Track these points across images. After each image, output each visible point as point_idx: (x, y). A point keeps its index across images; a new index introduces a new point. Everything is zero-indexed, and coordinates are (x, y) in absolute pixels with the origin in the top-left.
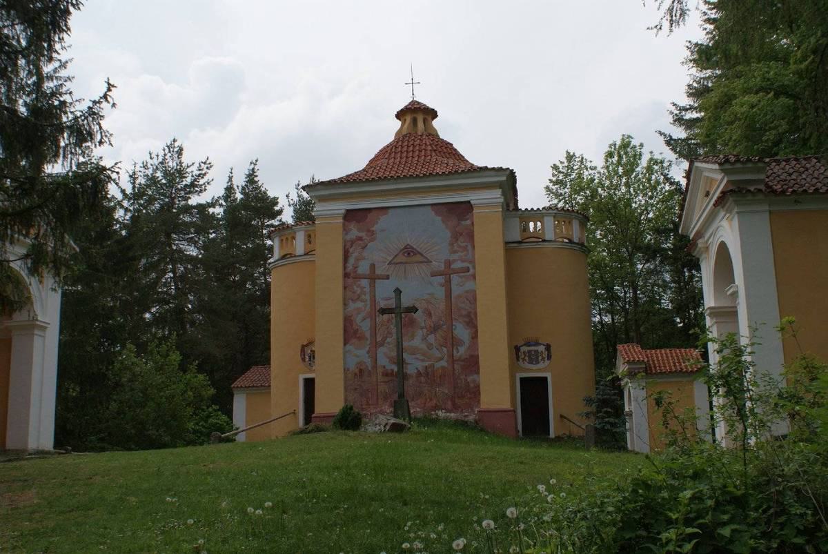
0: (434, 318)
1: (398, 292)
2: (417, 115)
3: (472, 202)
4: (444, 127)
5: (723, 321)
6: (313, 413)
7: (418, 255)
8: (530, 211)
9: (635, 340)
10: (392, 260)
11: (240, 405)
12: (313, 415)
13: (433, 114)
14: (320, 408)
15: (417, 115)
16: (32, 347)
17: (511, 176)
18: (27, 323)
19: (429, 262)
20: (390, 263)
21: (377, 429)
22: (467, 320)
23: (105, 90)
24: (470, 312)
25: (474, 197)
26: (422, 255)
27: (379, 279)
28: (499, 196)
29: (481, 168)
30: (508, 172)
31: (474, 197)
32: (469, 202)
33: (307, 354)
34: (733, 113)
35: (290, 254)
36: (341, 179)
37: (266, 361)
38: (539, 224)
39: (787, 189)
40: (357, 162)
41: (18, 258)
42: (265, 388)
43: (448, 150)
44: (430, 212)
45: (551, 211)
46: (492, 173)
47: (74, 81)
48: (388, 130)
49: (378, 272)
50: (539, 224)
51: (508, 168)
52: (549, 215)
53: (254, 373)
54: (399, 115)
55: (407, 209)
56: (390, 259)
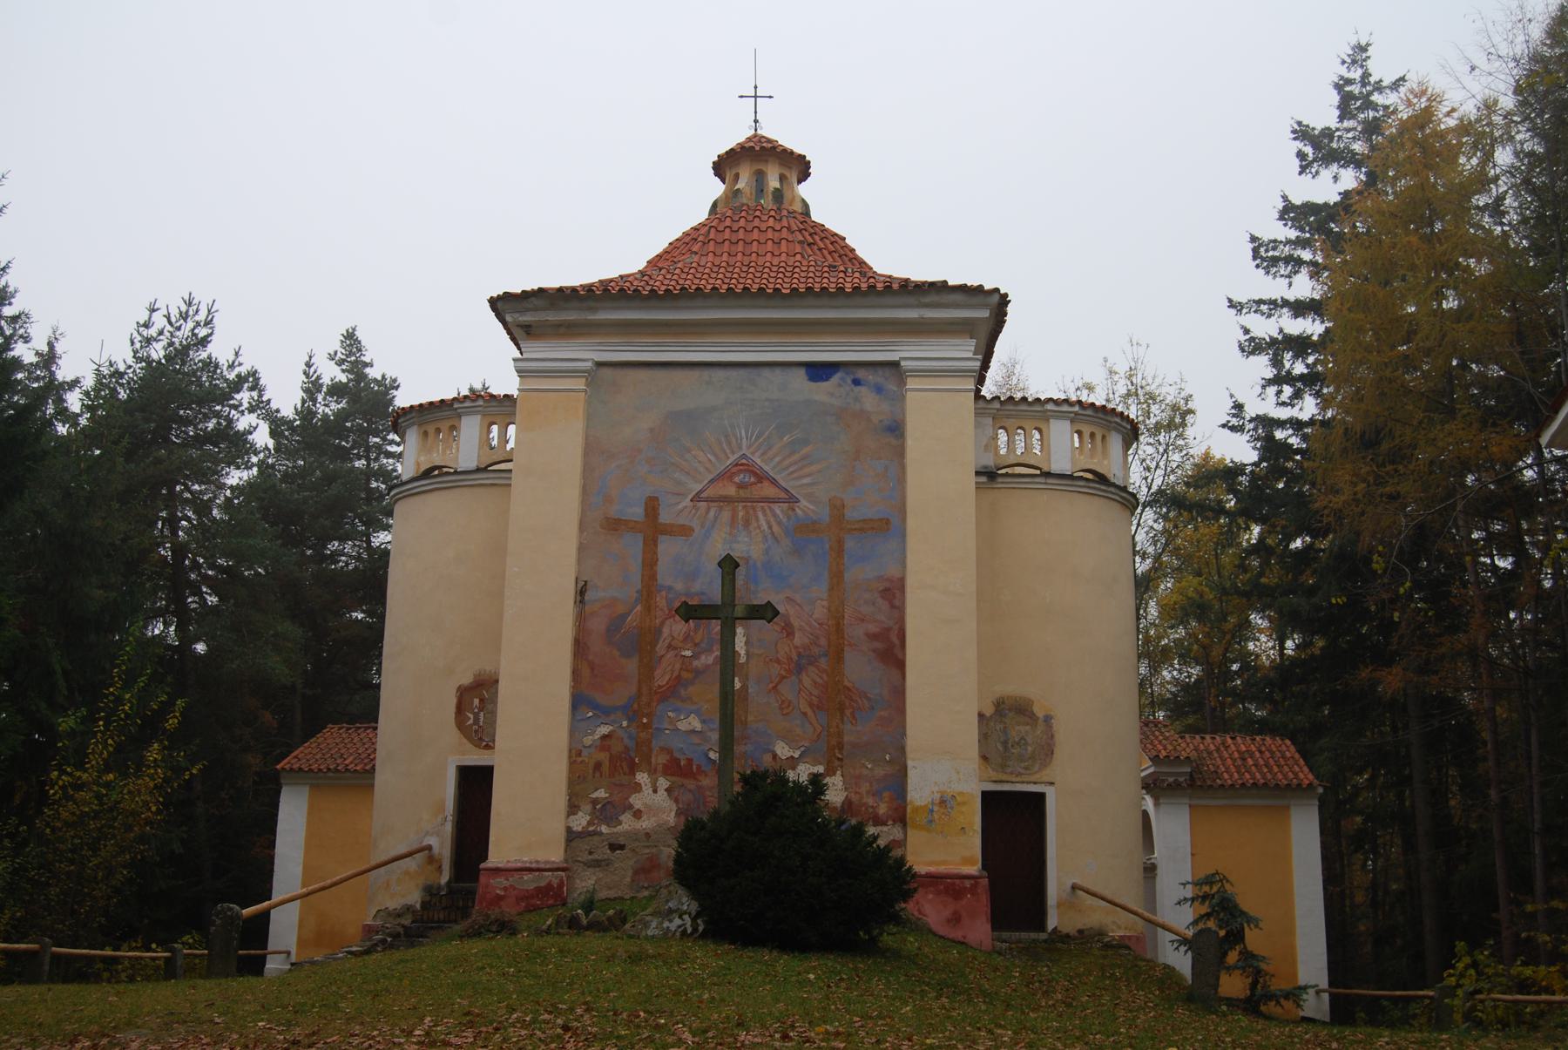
0: (798, 639)
1: (729, 565)
2: (761, 169)
3: (903, 363)
4: (823, 198)
6: (485, 858)
7: (766, 484)
8: (1031, 404)
10: (701, 491)
11: (293, 815)
12: (482, 866)
13: (801, 167)
14: (504, 848)
15: (761, 169)
17: (1004, 301)
19: (792, 500)
20: (697, 498)
21: (673, 926)
22: (878, 645)
24: (889, 629)
25: (907, 352)
26: (774, 482)
28: (970, 355)
30: (996, 298)
32: (895, 365)
33: (476, 702)
35: (440, 468)
36: (589, 288)
37: (369, 715)
40: (625, 256)
42: (361, 777)
43: (835, 248)
44: (802, 372)
45: (1065, 408)
48: (695, 197)
49: (665, 517)
51: (997, 290)
52: (1061, 416)
53: (332, 742)
54: (722, 166)
55: (742, 372)
56: (698, 487)
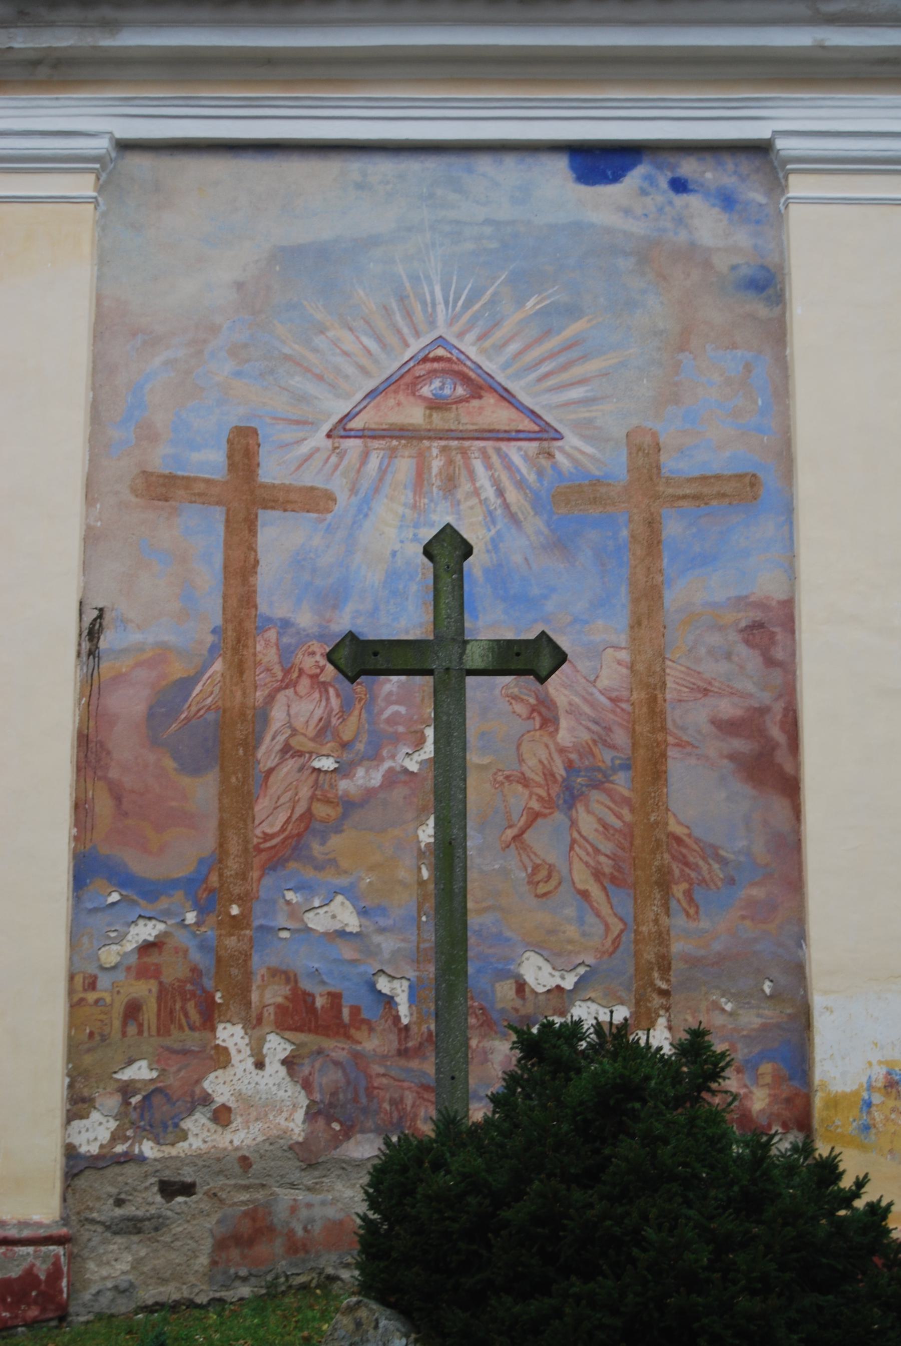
26: (507, 397)
44: (561, 164)
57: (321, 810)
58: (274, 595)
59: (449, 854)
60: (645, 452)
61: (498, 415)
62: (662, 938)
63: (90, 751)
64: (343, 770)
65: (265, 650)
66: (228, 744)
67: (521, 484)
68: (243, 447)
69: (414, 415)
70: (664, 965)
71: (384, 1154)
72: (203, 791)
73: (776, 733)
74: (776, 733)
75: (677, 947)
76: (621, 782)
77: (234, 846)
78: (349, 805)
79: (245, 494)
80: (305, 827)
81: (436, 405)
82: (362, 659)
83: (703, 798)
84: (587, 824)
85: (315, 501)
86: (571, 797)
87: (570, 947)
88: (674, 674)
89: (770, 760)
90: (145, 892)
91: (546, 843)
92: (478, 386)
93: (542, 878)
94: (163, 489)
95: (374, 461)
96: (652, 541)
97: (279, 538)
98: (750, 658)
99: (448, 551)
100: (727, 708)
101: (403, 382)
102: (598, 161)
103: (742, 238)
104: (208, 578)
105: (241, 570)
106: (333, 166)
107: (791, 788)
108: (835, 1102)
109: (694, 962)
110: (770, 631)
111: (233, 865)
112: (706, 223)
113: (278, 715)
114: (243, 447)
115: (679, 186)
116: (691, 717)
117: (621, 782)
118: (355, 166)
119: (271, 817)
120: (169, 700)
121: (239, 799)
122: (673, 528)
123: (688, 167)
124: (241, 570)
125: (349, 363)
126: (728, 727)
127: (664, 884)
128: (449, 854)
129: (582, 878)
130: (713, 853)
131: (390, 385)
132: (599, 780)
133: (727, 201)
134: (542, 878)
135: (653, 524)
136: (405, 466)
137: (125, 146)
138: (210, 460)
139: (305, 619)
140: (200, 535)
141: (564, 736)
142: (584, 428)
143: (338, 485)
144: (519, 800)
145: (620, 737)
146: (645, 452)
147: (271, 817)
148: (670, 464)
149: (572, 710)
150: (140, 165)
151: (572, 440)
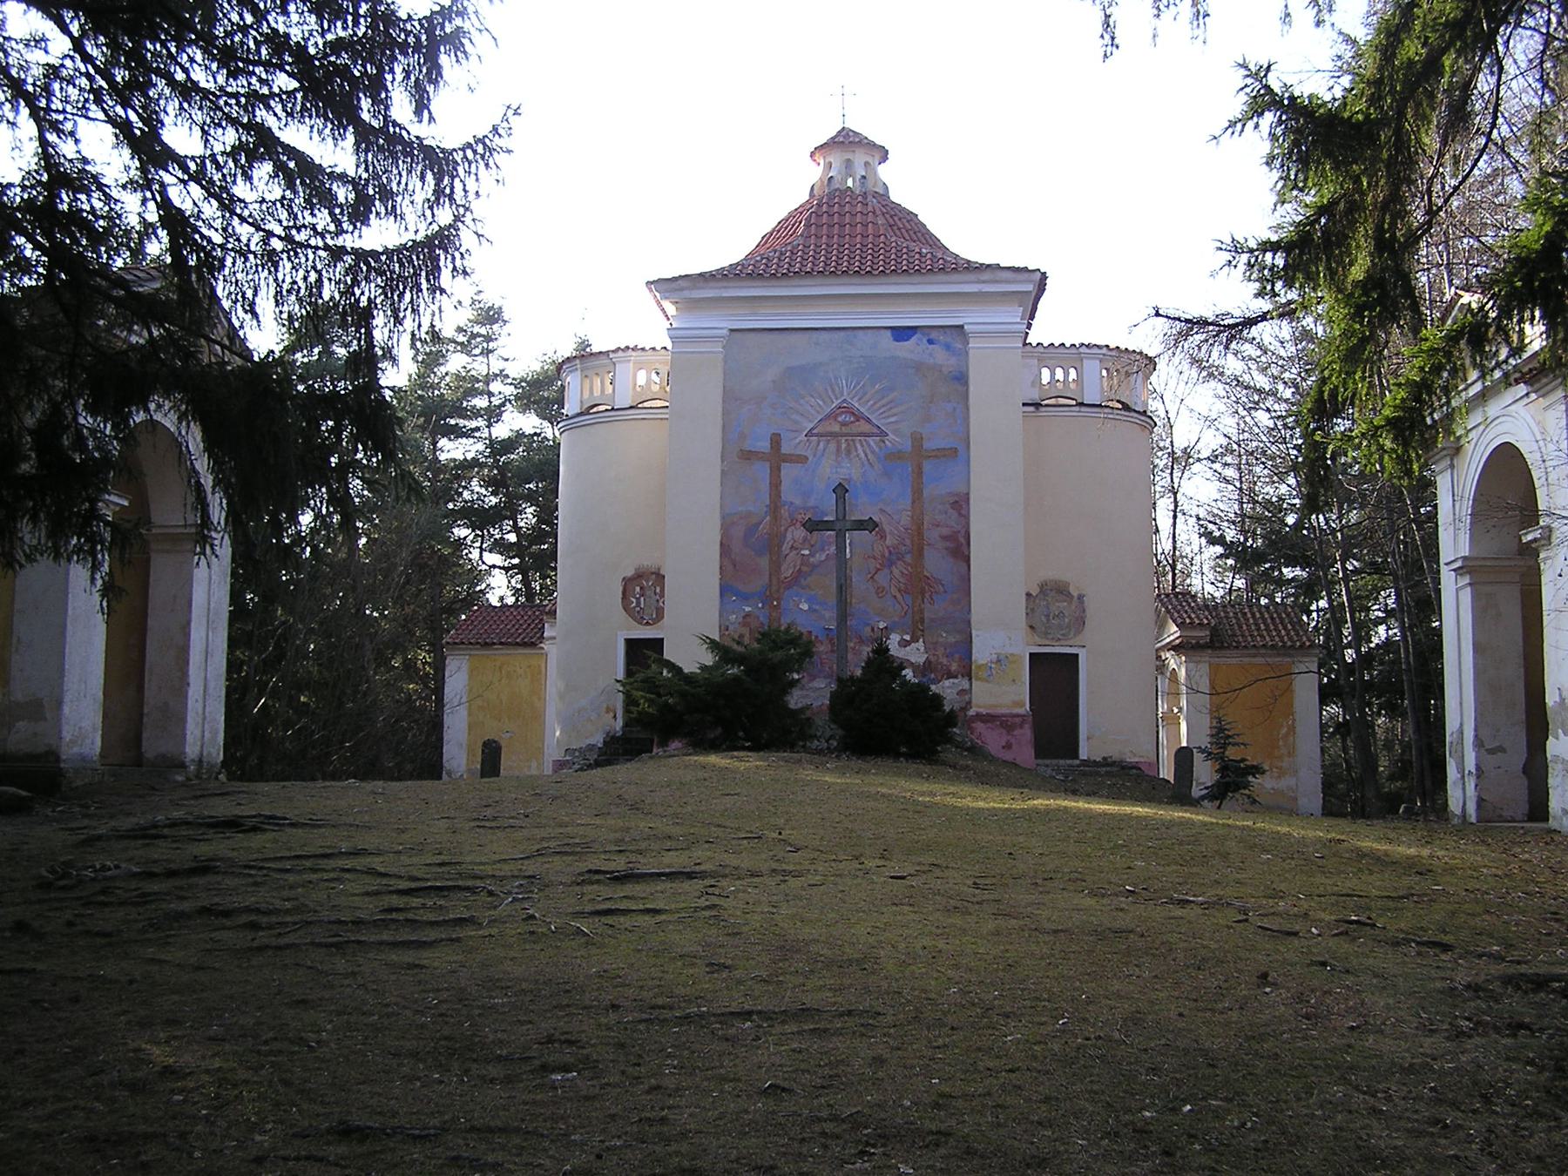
5: (211, 685)
9: (1532, 563)
16: (189, 582)
17: (1044, 276)
18: (179, 530)
23: (18, 37)
25: (970, 318)
26: (868, 420)
27: (791, 461)
29: (989, 266)
31: (970, 318)
34: (111, 219)
38: (1072, 371)
39: (488, 379)
41: (1255, 331)
43: (906, 225)
44: (889, 333)
46: (1009, 275)
47: (1257, 59)
48: (792, 184)
50: (1072, 371)
52: (1092, 357)
57: (805, 569)
58: (788, 493)
59: (843, 588)
60: (917, 440)
61: (866, 428)
62: (922, 611)
63: (725, 549)
64: (812, 555)
65: (784, 512)
66: (773, 545)
67: (873, 452)
68: (776, 440)
69: (836, 428)
70: (922, 621)
71: (1521, 313)
72: (764, 562)
73: (962, 540)
74: (962, 540)
75: (926, 615)
76: (908, 558)
77: (775, 581)
78: (814, 567)
79: (776, 457)
80: (799, 575)
81: (844, 424)
82: (814, 526)
83: (936, 563)
84: (896, 571)
85: (801, 459)
86: (891, 564)
87: (142, 1128)
88: (926, 518)
89: (959, 549)
90: (745, 598)
91: (882, 578)
92: (859, 417)
93: (880, 591)
94: (748, 456)
95: (822, 445)
96: (919, 472)
97: (788, 472)
98: (954, 514)
99: (841, 490)
100: (945, 531)
101: (832, 416)
102: (902, 333)
103: (953, 361)
104: (765, 486)
105: (775, 485)
106: (807, 334)
107: (967, 560)
108: (979, 667)
109: (932, 620)
110: (960, 504)
111: (774, 588)
112: (939, 356)
113: (789, 536)
114: (776, 440)
115: (930, 342)
116: (932, 535)
117: (908, 558)
118: (815, 335)
119: (787, 572)
120: (751, 530)
121: (776, 566)
122: (927, 467)
123: (934, 335)
124: (775, 485)
125: (812, 410)
126: (945, 538)
127: (923, 593)
128: (843, 588)
129: (894, 591)
130: (940, 582)
131: (828, 417)
132: (901, 558)
133: (948, 347)
134: (880, 591)
135: (920, 467)
136: (832, 446)
137: (732, 330)
138: (764, 445)
139: (798, 502)
140: (762, 471)
141: (888, 542)
142: (895, 432)
143: (809, 454)
144: (873, 565)
145: (908, 542)
146: (917, 440)
147: (787, 572)
148: (926, 445)
149: (891, 533)
150: (738, 335)
151: (891, 436)
